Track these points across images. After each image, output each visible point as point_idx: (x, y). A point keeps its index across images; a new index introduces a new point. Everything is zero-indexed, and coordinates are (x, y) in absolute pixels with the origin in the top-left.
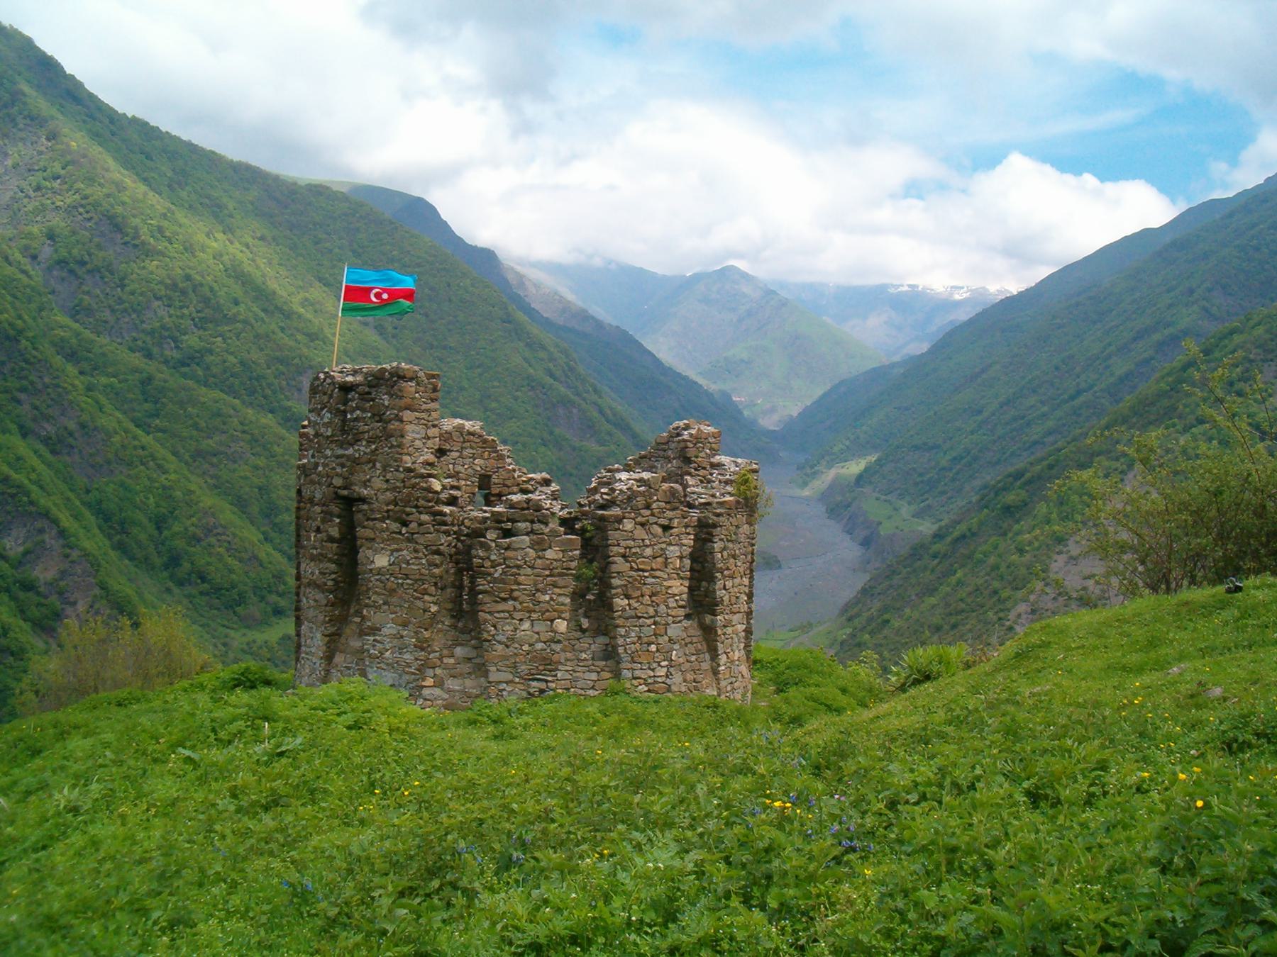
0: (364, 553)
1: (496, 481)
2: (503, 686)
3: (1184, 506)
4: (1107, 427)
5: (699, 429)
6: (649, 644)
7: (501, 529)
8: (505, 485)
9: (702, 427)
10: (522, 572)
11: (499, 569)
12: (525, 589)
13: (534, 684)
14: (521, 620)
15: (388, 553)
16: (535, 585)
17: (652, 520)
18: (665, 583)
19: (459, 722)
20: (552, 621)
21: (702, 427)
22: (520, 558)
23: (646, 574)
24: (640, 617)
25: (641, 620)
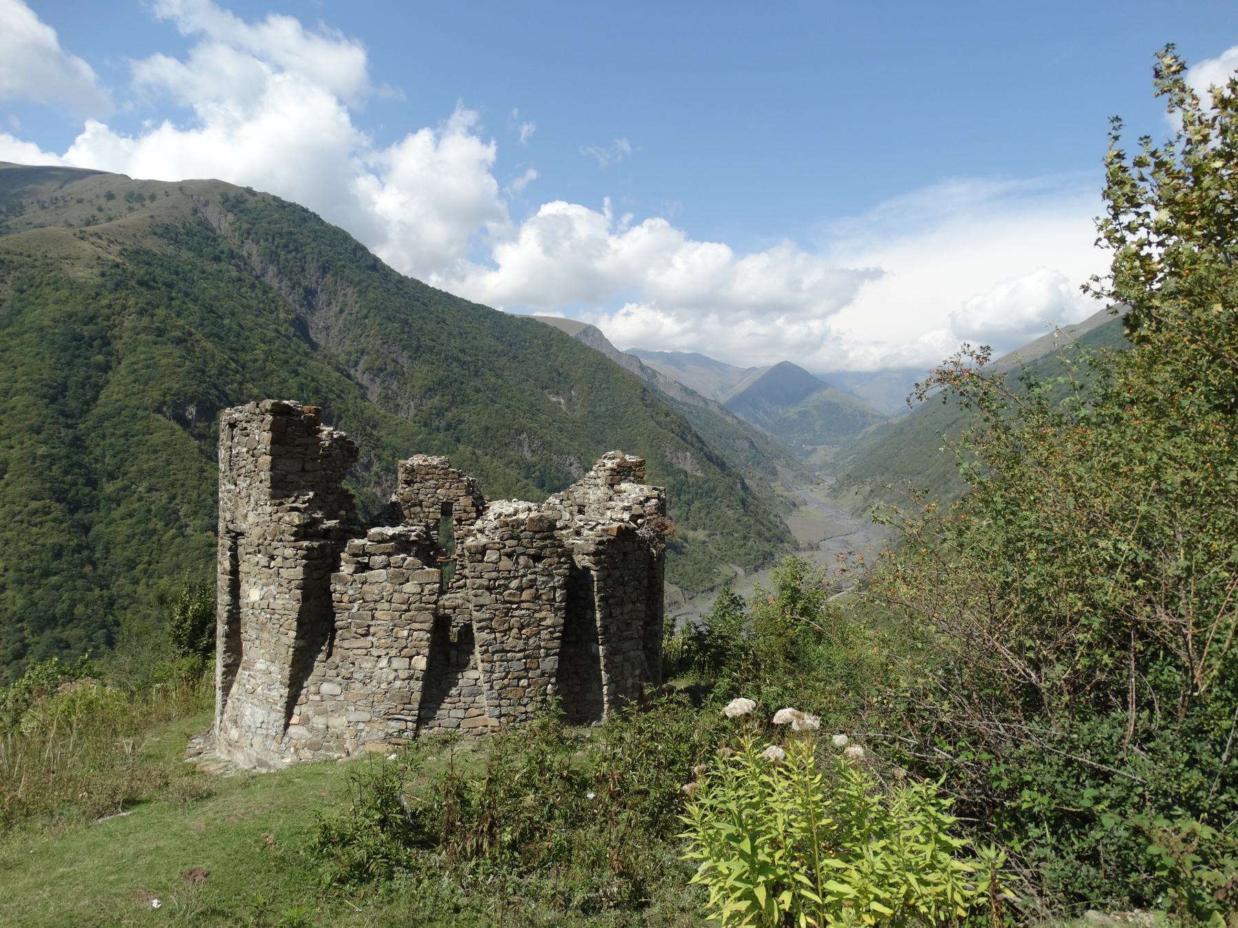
0: (244, 587)
1: (458, 508)
2: (361, 726)
3: (899, 545)
4: (1171, 458)
5: (623, 459)
6: (519, 679)
7: (358, 562)
8: (465, 511)
9: (627, 457)
10: (379, 606)
11: (356, 605)
12: (382, 625)
13: (393, 724)
14: (379, 657)
15: (260, 587)
16: (392, 620)
17: (520, 550)
18: (537, 615)
19: (30, 692)
20: (411, 658)
21: (627, 457)
22: (377, 592)
23: (514, 606)
24: (509, 651)
25: (509, 655)
